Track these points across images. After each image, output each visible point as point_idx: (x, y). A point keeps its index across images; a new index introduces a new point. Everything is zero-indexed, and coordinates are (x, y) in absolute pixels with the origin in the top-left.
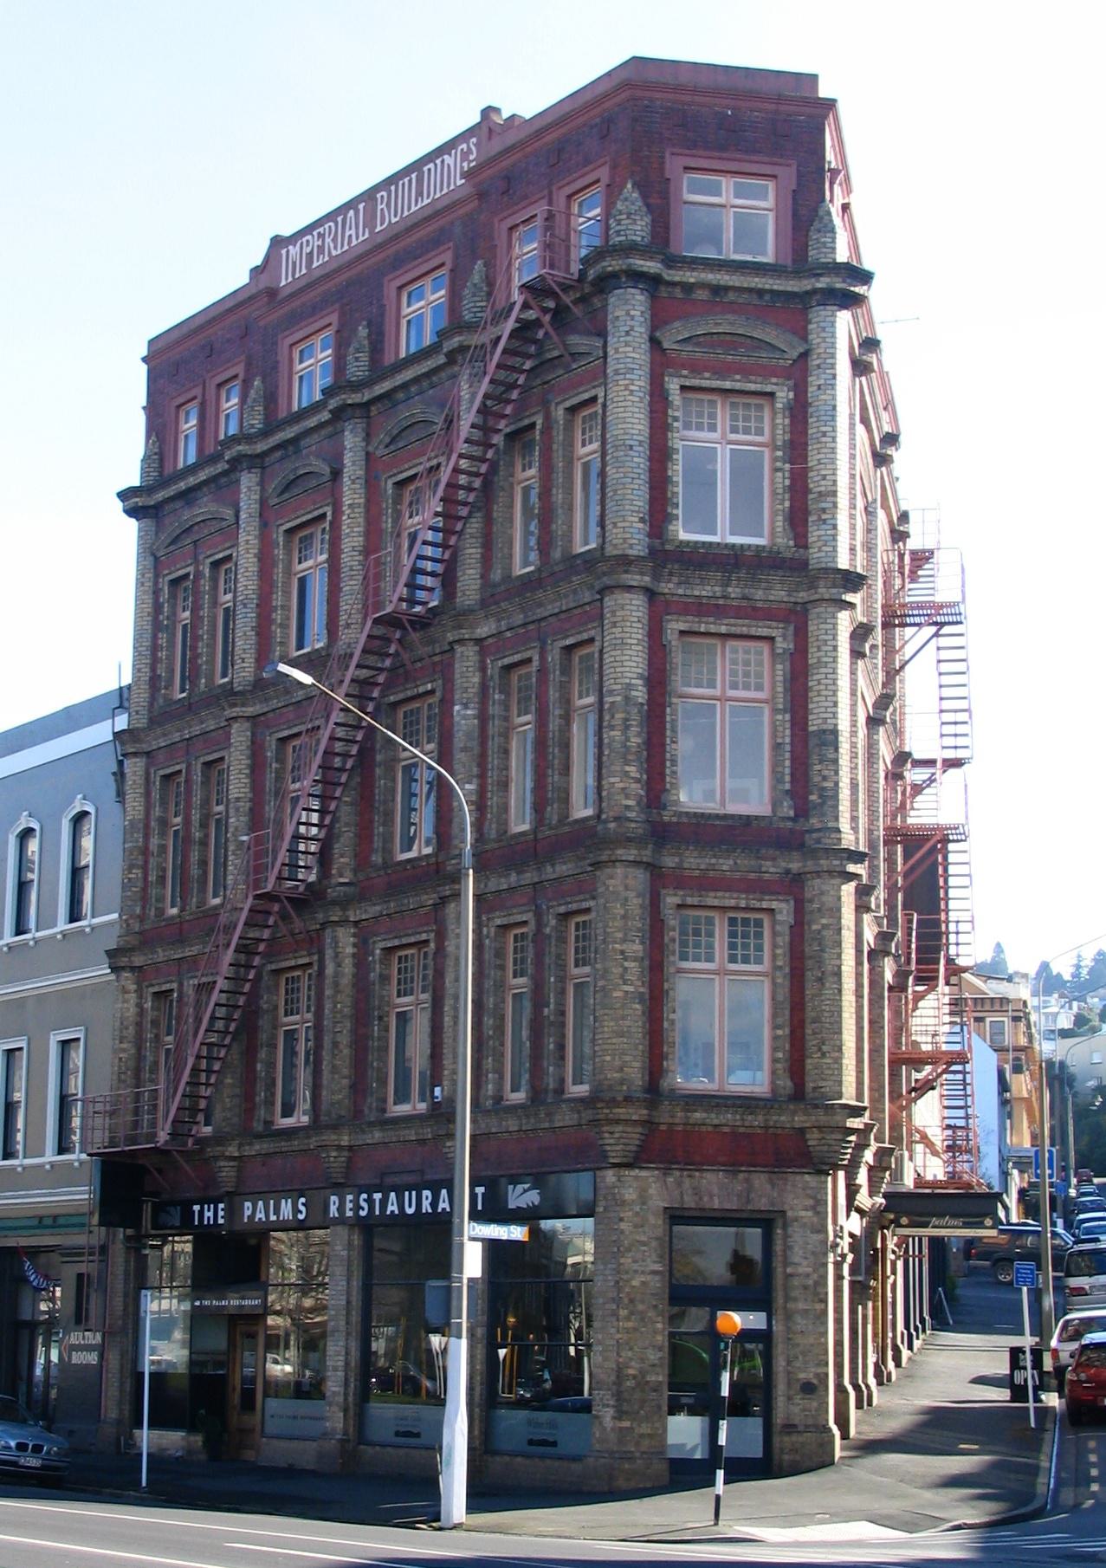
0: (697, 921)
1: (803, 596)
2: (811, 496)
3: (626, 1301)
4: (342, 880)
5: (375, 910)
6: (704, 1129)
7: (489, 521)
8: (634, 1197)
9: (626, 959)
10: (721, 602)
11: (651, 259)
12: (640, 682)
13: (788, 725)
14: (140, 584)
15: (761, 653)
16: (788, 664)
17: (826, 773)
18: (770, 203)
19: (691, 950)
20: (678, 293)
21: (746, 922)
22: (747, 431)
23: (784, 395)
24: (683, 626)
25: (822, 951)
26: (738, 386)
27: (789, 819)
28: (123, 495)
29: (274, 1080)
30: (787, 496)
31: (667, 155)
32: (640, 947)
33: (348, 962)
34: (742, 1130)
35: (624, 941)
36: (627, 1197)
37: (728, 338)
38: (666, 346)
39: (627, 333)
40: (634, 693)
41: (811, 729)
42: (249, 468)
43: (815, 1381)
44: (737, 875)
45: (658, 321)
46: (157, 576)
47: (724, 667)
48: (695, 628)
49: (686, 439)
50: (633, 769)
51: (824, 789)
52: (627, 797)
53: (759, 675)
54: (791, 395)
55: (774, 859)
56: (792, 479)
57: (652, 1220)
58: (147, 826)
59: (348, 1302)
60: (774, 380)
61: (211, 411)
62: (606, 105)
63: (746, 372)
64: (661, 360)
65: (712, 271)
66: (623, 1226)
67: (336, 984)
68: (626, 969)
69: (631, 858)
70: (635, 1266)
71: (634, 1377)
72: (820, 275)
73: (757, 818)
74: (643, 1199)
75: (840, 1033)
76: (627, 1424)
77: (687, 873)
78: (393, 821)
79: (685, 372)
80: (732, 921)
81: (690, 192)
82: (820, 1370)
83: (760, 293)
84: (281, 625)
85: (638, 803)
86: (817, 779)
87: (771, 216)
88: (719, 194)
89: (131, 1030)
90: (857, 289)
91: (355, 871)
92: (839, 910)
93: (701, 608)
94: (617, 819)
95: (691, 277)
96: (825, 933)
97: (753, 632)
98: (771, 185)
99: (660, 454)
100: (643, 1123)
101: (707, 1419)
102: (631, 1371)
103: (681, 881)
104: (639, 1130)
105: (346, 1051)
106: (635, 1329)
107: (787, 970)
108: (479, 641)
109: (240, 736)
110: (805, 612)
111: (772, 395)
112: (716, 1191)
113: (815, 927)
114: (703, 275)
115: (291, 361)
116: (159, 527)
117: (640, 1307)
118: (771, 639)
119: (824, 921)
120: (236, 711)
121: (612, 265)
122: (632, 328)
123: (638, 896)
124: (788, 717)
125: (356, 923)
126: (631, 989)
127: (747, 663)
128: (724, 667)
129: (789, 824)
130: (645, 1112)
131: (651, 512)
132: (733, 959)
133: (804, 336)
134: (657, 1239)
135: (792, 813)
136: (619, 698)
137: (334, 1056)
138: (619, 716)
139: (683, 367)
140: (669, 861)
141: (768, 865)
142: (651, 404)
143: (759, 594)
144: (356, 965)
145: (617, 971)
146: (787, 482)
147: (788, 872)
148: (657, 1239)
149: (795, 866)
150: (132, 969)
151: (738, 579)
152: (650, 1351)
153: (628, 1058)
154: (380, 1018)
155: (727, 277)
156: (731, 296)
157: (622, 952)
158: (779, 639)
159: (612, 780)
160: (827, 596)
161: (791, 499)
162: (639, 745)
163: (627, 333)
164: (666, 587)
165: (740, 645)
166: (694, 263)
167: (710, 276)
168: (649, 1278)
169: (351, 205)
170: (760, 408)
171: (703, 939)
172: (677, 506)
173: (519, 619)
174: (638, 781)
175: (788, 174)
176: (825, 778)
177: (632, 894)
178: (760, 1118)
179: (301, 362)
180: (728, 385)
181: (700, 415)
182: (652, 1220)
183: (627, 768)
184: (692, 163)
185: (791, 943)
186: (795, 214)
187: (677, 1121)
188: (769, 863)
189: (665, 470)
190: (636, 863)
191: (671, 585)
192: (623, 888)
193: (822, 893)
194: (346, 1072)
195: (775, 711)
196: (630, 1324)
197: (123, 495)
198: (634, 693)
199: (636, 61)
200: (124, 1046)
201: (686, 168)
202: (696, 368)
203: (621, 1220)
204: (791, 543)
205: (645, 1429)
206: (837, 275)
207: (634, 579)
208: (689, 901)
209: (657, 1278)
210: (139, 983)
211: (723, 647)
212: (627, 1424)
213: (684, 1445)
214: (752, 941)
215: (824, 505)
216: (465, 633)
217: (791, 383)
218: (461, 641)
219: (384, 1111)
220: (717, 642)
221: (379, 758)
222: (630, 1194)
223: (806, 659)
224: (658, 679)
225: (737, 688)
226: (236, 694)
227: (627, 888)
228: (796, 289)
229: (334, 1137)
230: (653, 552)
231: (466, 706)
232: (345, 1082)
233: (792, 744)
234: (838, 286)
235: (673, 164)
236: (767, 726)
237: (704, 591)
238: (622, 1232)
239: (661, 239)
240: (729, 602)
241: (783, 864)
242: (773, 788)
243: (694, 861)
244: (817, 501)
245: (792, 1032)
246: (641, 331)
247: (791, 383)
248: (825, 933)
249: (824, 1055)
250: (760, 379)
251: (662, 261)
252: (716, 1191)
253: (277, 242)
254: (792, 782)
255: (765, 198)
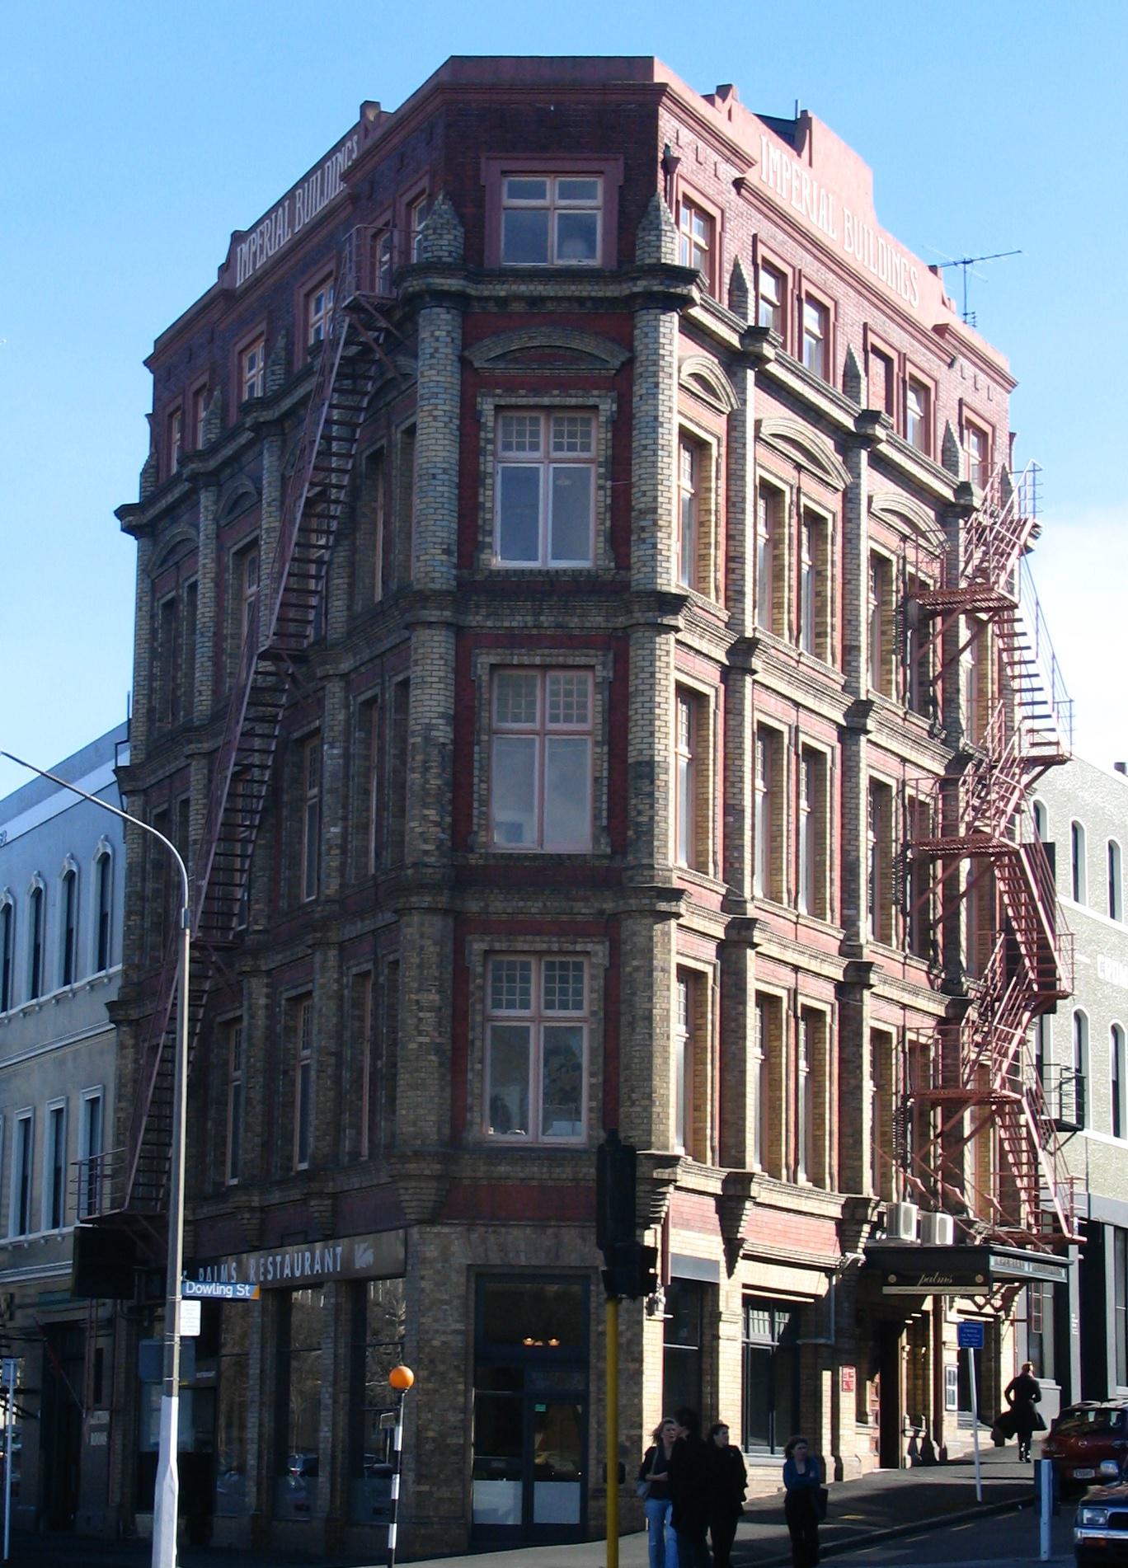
0: (511, 965)
1: (621, 621)
2: (634, 514)
3: (426, 1361)
4: (257, 928)
5: (279, 958)
6: (510, 1182)
7: (354, 550)
8: (436, 1254)
9: (421, 1009)
10: (534, 632)
11: (452, 276)
12: (441, 721)
13: (606, 758)
14: (139, 609)
15: (585, 682)
16: (607, 693)
17: (641, 807)
18: (598, 201)
19: (504, 997)
20: (492, 307)
21: (564, 966)
22: (572, 447)
23: (608, 407)
24: (493, 660)
25: (634, 994)
26: (557, 401)
27: (605, 856)
28: (122, 512)
29: (224, 1138)
30: (608, 515)
31: (483, 160)
32: (437, 997)
33: (261, 1013)
34: (550, 1183)
35: (419, 990)
36: (428, 1255)
37: (547, 351)
38: (477, 365)
39: (432, 356)
40: (434, 733)
41: (630, 761)
42: (207, 486)
43: (628, 1444)
44: (548, 918)
45: (469, 337)
46: (153, 600)
47: (544, 699)
48: (508, 660)
49: (505, 458)
50: (433, 812)
51: (639, 824)
52: (425, 841)
53: (583, 706)
54: (614, 407)
55: (586, 899)
56: (613, 497)
57: (454, 1277)
58: (144, 869)
59: (262, 1371)
60: (595, 392)
61: (189, 421)
62: (429, 108)
63: (564, 386)
64: (472, 382)
65: (524, 283)
66: (423, 1284)
67: (250, 1037)
68: (420, 1020)
69: (425, 905)
70: (436, 1326)
71: (434, 1440)
72: (638, 278)
73: (569, 856)
74: (445, 1256)
75: (650, 1079)
76: (425, 1488)
77: (494, 917)
78: (300, 864)
79: (498, 391)
80: (550, 966)
81: (511, 196)
82: (633, 1432)
83: (580, 301)
84: (231, 656)
85: (438, 848)
86: (633, 813)
87: (599, 215)
88: (542, 196)
89: (129, 1089)
90: (679, 290)
91: (269, 917)
92: (651, 951)
93: (512, 640)
94: (415, 865)
95: (502, 291)
96: (635, 975)
97: (570, 661)
98: (600, 183)
99: (469, 480)
100: (439, 1178)
101: (519, 1484)
102: (431, 1434)
103: (486, 926)
104: (435, 1184)
105: (259, 1108)
106: (436, 1391)
107: (602, 1014)
108: (344, 676)
109: (197, 774)
110: (627, 638)
111: (596, 407)
112: (522, 1247)
113: (628, 969)
114: (514, 287)
115: (240, 368)
116: (155, 543)
117: (442, 1368)
118: (591, 667)
119: (635, 963)
120: (192, 748)
121: (414, 285)
122: (436, 350)
123: (435, 944)
124: (606, 749)
125: (269, 973)
126: (427, 1040)
127: (569, 694)
128: (544, 699)
129: (605, 862)
130: (438, 1166)
131: (460, 543)
132: (550, 1005)
133: (627, 342)
134: (459, 1297)
135: (609, 850)
136: (419, 739)
137: (247, 1113)
138: (419, 758)
139: (498, 385)
140: (474, 906)
141: (579, 906)
142: (460, 428)
143: (574, 622)
144: (267, 1017)
145: (412, 1021)
146: (609, 501)
147: (601, 912)
148: (459, 1297)
149: (609, 906)
150: (130, 1023)
151: (550, 608)
152: (451, 1413)
153: (422, 1112)
154: (285, 1073)
155: (541, 288)
156: (550, 306)
157: (417, 1002)
158: (599, 667)
159: (413, 824)
160: (642, 621)
161: (612, 519)
162: (439, 787)
163: (432, 356)
164: (474, 620)
165: (561, 674)
166: (505, 275)
167: (523, 288)
168: (450, 1338)
169: (279, 203)
170: (587, 422)
171: (518, 985)
172: (491, 533)
173: (366, 655)
174: (437, 824)
175: (616, 169)
176: (640, 813)
177: (429, 942)
178: (569, 1170)
179: (250, 369)
180: (546, 401)
181: (521, 434)
182: (454, 1277)
183: (426, 812)
184: (507, 166)
185: (606, 986)
186: (622, 213)
187: (480, 1174)
188: (581, 904)
189: (476, 495)
190: (428, 910)
191: (479, 618)
192: (421, 937)
193: (634, 934)
194: (259, 1129)
195: (596, 744)
196: (430, 1386)
197: (122, 512)
198: (434, 733)
199: (456, 63)
200: (123, 1105)
201: (505, 173)
202: (511, 387)
203: (422, 1278)
204: (612, 565)
205: (445, 1492)
206: (654, 277)
207: (433, 615)
208: (497, 946)
209: (459, 1338)
210: (136, 1037)
211: (544, 677)
212: (425, 1488)
213: (496, 1510)
214: (571, 986)
215: (643, 524)
216: (330, 669)
217: (614, 394)
218: (327, 677)
219: (290, 1169)
220: (537, 674)
221: (286, 798)
222: (431, 1251)
223: (627, 687)
224: (465, 717)
225: (558, 721)
226: (197, 729)
227: (422, 936)
228: (616, 294)
229: (245, 1198)
230: (461, 583)
231: (332, 747)
232: (257, 1140)
233: (610, 778)
234: (656, 288)
235: (490, 169)
236: (590, 759)
237: (516, 622)
238: (423, 1290)
239: (473, 258)
240: (543, 632)
241: (597, 905)
242: (594, 826)
243: (500, 905)
244: (638, 518)
245: (605, 1081)
246: (447, 352)
247: (614, 394)
248: (635, 975)
249: (633, 1104)
250: (580, 393)
251: (465, 278)
252: (522, 1247)
253: (237, 238)
254: (609, 818)
255: (594, 197)
